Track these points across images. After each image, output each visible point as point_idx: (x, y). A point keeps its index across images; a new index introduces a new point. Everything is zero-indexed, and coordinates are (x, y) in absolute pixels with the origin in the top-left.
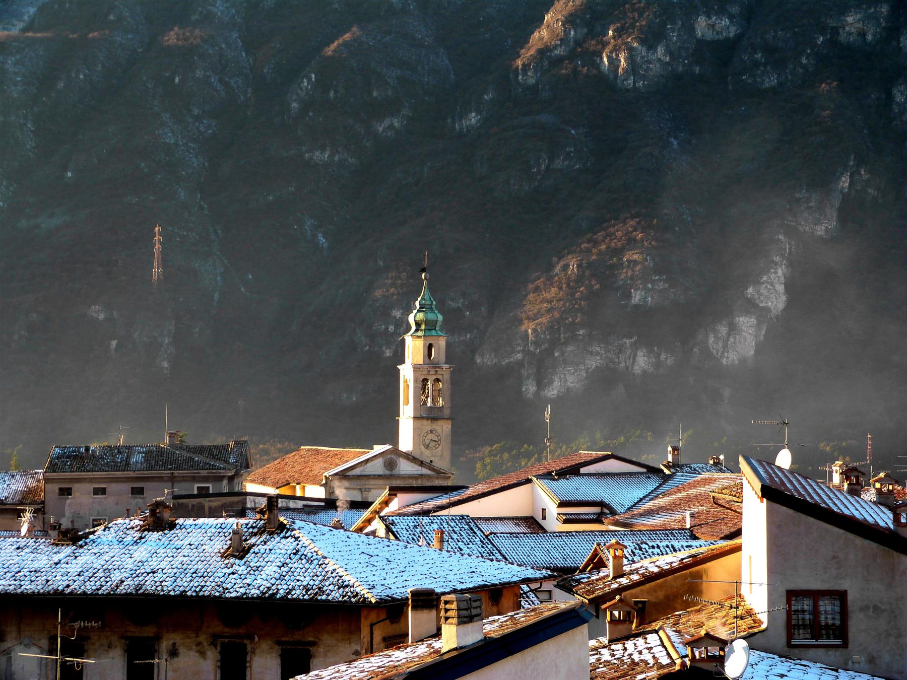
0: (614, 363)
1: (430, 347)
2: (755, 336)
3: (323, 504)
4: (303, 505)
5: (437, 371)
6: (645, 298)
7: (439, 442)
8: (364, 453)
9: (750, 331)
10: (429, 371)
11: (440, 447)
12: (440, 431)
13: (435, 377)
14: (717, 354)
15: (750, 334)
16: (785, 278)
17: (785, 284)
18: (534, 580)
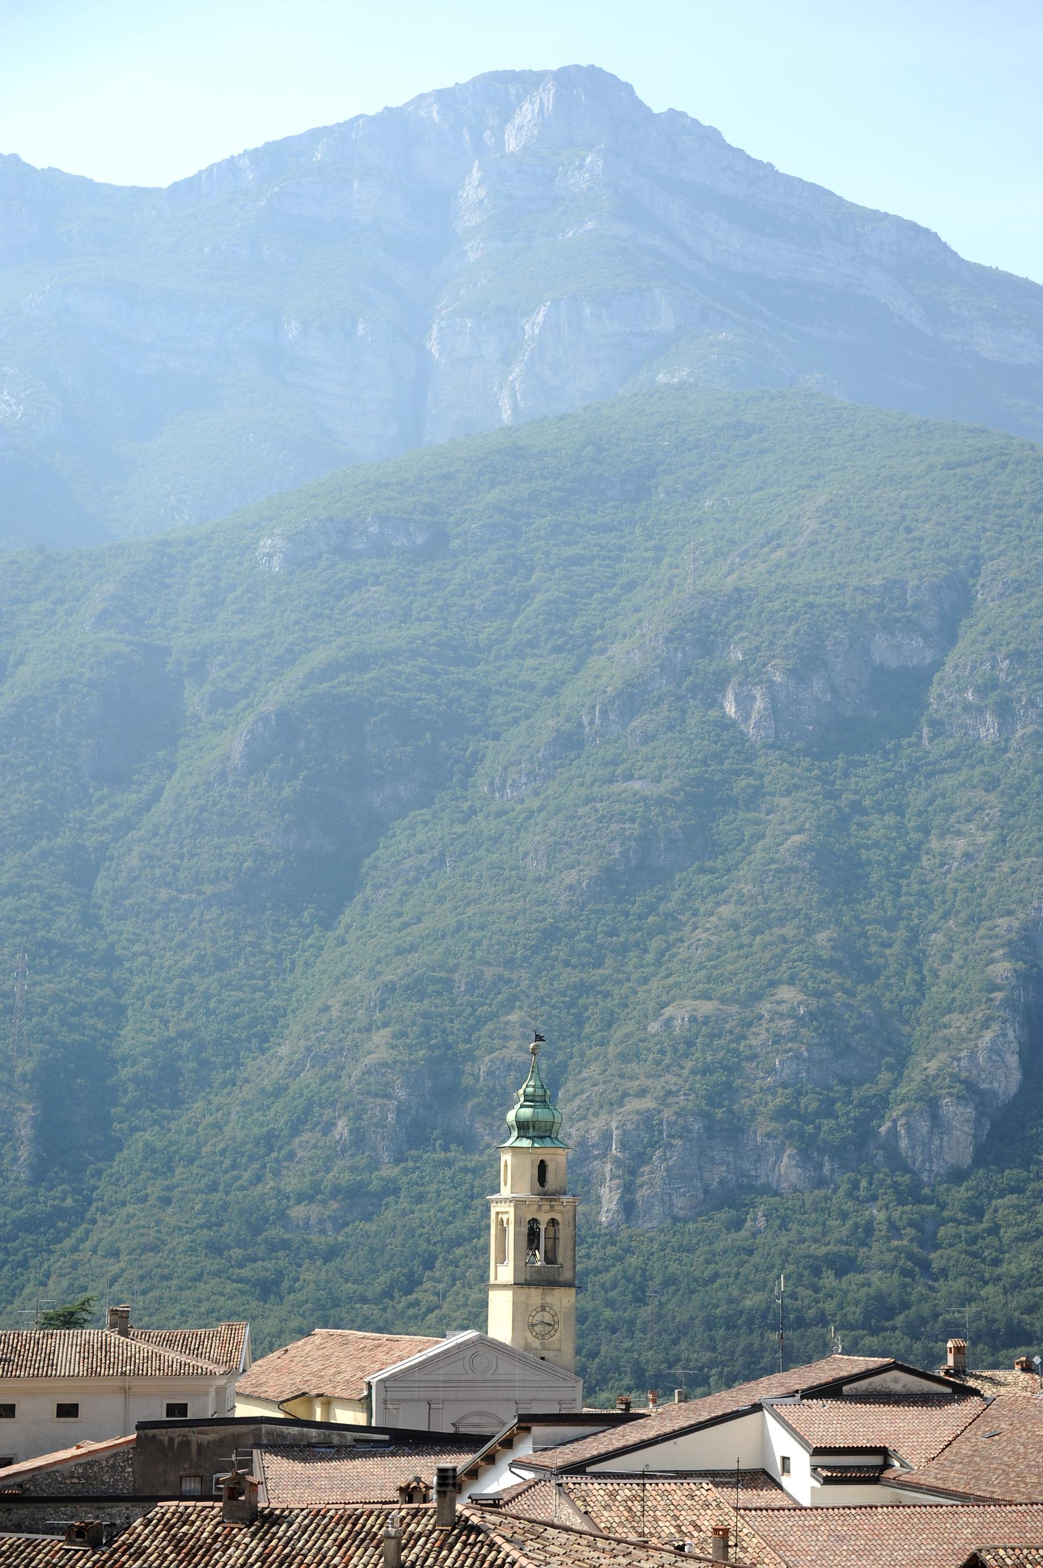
0: (747, 1176)
1: (542, 1167)
2: (974, 1137)
3: (387, 1437)
4: (355, 1440)
5: (552, 1206)
6: (797, 1073)
7: (556, 1326)
8: (437, 1342)
9: (966, 1129)
10: (540, 1206)
11: (558, 1335)
12: (557, 1308)
13: (549, 1216)
14: (914, 1164)
15: (966, 1133)
16: (1020, 1043)
17: (1020, 1054)
18: (292, 1446)
